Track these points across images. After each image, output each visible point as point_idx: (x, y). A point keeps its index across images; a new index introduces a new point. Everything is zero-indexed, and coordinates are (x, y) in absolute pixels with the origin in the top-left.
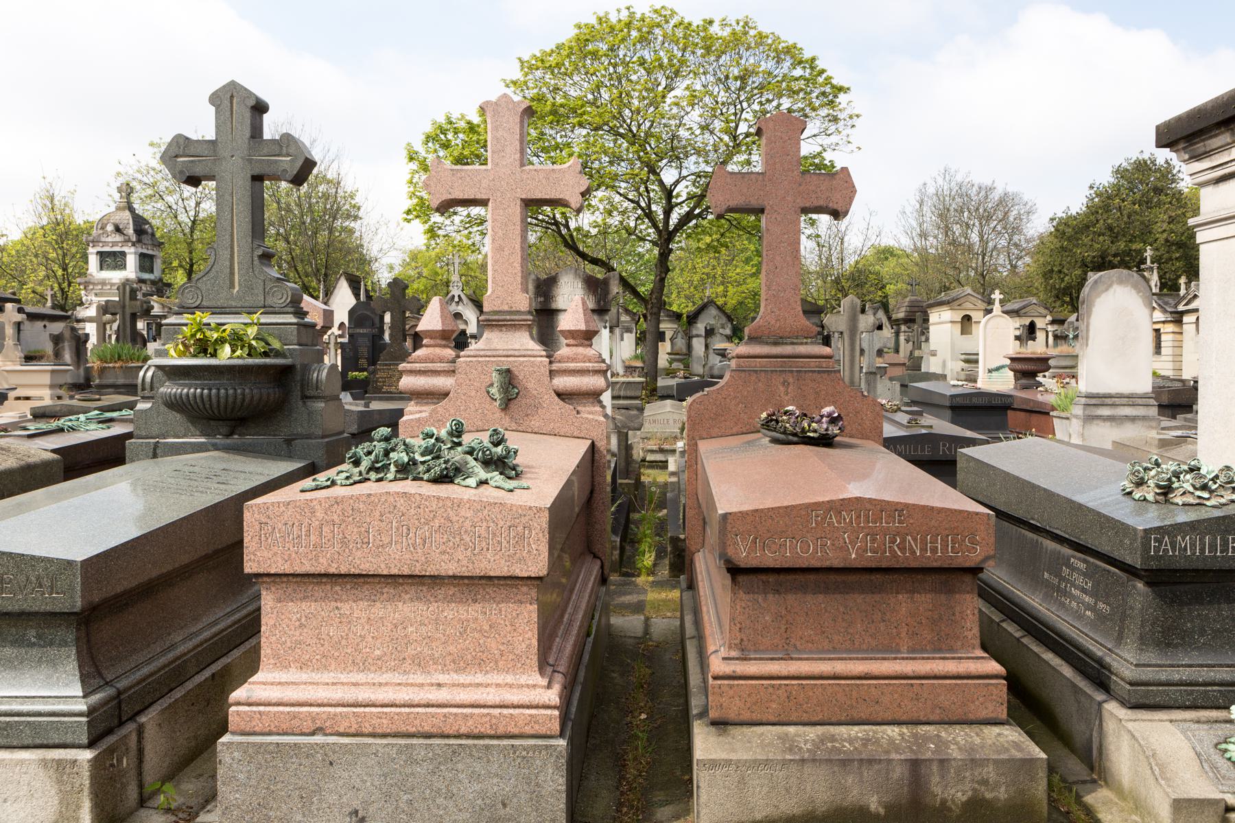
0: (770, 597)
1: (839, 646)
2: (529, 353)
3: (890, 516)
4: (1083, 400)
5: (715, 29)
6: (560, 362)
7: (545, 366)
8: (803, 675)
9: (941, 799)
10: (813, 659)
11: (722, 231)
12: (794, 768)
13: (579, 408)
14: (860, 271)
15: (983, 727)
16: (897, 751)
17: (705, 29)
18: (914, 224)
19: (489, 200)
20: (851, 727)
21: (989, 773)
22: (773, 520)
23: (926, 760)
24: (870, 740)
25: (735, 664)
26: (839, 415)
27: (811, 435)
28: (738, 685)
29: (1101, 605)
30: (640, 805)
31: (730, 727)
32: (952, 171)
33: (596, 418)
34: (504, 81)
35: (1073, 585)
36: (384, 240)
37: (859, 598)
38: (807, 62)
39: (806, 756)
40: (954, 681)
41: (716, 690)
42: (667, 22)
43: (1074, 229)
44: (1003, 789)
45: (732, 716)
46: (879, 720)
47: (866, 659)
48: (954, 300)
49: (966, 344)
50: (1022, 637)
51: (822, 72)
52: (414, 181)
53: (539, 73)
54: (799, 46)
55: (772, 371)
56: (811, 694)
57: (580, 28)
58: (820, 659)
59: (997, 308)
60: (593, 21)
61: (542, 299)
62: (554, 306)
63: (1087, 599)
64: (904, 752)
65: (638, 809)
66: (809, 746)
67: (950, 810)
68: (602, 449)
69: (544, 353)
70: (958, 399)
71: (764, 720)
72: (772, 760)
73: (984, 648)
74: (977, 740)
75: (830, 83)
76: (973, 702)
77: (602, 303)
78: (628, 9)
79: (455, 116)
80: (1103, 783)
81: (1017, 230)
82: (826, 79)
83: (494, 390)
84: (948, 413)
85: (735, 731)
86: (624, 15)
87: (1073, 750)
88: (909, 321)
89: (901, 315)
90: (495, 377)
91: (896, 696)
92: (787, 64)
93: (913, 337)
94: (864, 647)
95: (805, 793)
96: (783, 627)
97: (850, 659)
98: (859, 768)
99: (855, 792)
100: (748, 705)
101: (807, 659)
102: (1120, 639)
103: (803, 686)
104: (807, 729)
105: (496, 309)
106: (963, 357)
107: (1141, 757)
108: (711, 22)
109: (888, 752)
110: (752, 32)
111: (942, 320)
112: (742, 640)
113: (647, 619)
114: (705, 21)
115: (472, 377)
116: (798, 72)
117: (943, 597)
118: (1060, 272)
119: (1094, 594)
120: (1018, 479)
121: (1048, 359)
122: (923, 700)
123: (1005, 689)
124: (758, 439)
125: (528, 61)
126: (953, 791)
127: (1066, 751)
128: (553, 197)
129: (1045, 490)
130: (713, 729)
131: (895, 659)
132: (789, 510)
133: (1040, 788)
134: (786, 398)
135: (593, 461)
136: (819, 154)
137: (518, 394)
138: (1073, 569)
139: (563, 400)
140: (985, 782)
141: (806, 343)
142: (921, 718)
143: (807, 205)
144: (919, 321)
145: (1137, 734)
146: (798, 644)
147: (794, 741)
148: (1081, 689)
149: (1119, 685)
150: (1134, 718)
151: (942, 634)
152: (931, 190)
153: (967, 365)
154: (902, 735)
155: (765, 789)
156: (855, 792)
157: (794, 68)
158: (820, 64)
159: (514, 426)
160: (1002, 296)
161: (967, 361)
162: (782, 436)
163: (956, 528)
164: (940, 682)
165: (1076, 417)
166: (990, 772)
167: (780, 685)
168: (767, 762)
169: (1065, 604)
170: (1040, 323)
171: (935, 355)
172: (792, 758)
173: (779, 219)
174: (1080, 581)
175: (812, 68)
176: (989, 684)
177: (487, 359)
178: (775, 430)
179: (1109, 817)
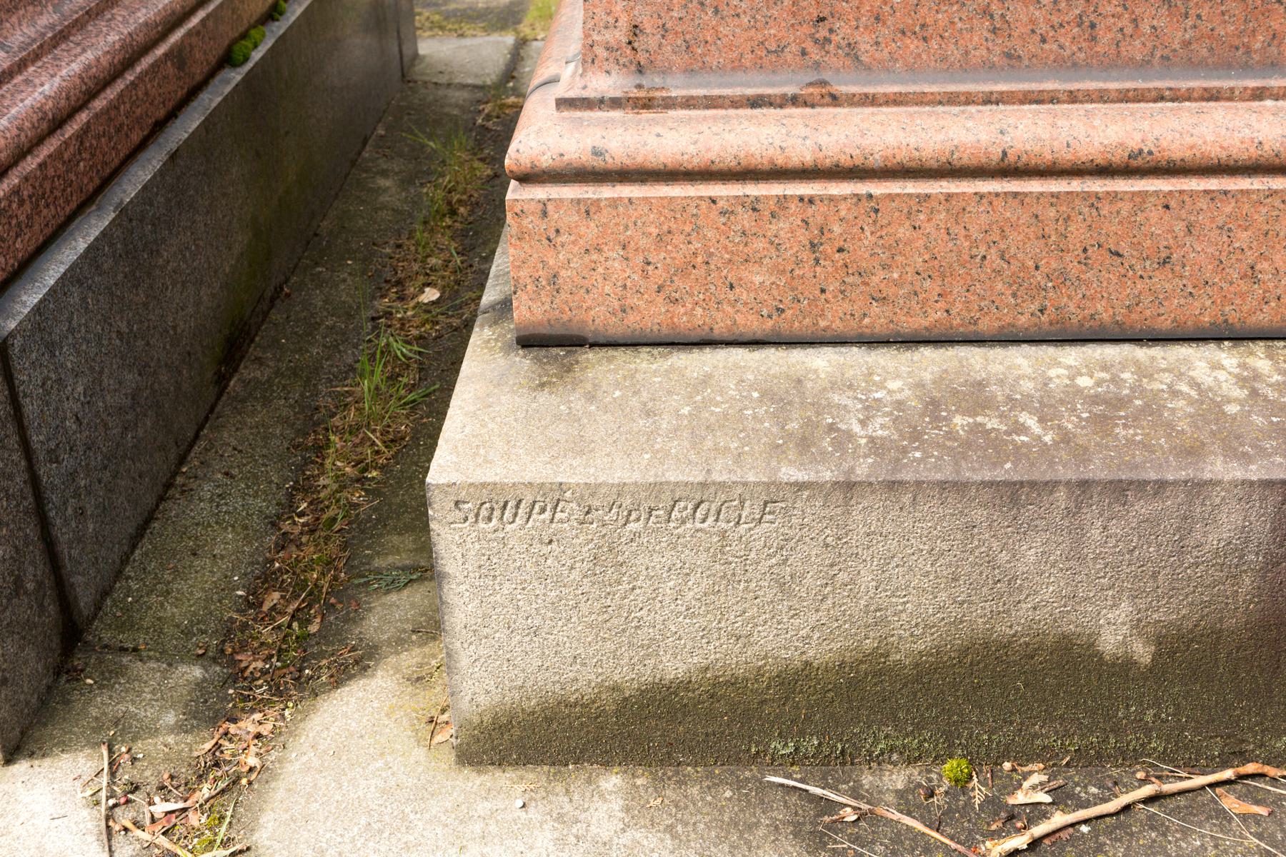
1: (1033, 46)
8: (876, 161)
10: (921, 100)
12: (809, 510)
16: (1233, 450)
20: (1050, 350)
24: (1121, 402)
25: (606, 124)
28: (614, 203)
30: (325, 583)
31: (590, 355)
39: (863, 469)
46: (1165, 324)
56: (904, 232)
58: (951, 99)
64: (1262, 452)
65: (313, 598)
66: (880, 427)
72: (722, 485)
85: (597, 366)
91: (1242, 238)
94: (1136, 49)
95: (853, 596)
97: (1073, 98)
99: (1047, 593)
100: (658, 276)
101: (897, 101)
103: (874, 206)
104: (882, 358)
109: (1193, 452)
112: (635, 29)
113: (522, 43)
130: (523, 362)
131: (1259, 95)
146: (864, 43)
154: (1249, 380)
167: (783, 200)
172: (802, 476)
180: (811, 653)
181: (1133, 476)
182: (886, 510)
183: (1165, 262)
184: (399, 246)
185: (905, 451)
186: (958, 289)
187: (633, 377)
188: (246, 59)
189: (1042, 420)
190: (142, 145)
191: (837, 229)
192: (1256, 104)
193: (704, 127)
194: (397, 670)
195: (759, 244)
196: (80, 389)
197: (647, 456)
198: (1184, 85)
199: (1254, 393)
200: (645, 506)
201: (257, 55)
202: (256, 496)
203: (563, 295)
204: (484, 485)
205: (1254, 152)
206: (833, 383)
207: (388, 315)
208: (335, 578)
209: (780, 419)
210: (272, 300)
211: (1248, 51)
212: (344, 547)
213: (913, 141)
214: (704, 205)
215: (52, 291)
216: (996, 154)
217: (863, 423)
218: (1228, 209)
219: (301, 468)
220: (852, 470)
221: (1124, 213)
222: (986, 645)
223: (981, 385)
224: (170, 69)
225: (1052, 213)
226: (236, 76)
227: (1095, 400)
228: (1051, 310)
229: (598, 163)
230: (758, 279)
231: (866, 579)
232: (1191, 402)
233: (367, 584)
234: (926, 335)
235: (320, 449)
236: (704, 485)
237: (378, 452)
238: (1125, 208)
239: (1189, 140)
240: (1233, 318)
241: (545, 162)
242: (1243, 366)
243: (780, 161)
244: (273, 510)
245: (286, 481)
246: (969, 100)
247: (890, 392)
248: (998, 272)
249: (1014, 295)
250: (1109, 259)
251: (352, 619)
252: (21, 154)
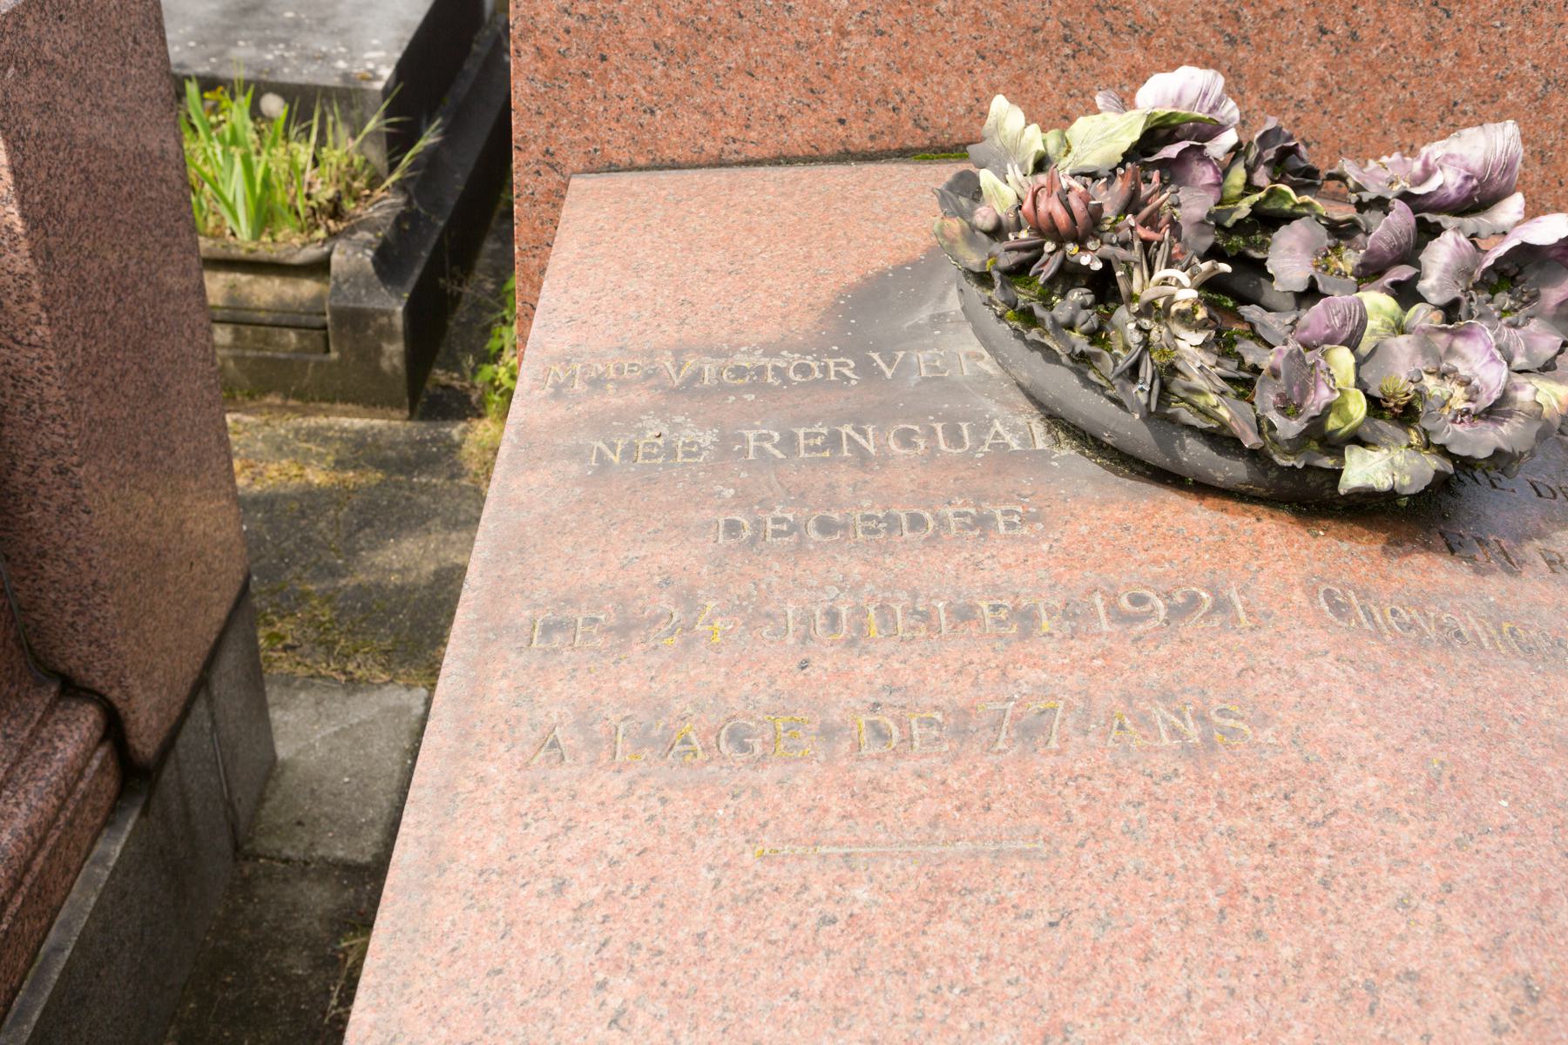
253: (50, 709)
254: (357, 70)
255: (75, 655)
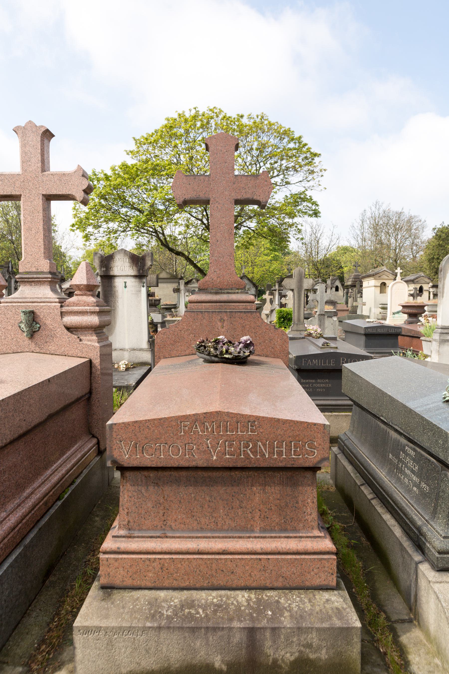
0: (151, 488)
2: (47, 300)
3: (244, 426)
4: (440, 330)
5: (245, 121)
6: (68, 306)
7: (57, 309)
8: (173, 551)
9: (273, 659)
10: (183, 537)
11: (250, 236)
12: (152, 633)
13: (82, 338)
14: (328, 259)
15: (316, 592)
17: (238, 120)
18: (359, 233)
19: (21, 195)
21: (312, 638)
22: (150, 429)
23: (260, 628)
26: (251, 342)
27: (227, 356)
28: (121, 559)
29: (423, 485)
30: (56, 643)
31: (115, 591)
32: (380, 203)
33: (93, 344)
34: (126, 151)
35: (406, 466)
36: (68, 243)
37: (222, 490)
38: (296, 139)
40: (294, 557)
41: (105, 562)
42: (217, 116)
43: (446, 234)
44: (324, 651)
45: (117, 582)
46: (234, 586)
47: (226, 537)
48: (376, 274)
49: (382, 298)
50: (372, 499)
51: (306, 145)
52: (76, 208)
53: (145, 147)
54: (292, 130)
55: (213, 312)
57: (168, 120)
58: (190, 537)
59: (399, 277)
60: (176, 116)
61: (104, 269)
62: (112, 273)
63: (415, 478)
67: (280, 667)
68: (97, 365)
69: (57, 300)
70: (369, 330)
71: (143, 585)
72: (134, 627)
73: (321, 528)
74: (308, 607)
75: (310, 151)
76: (309, 573)
77: (141, 271)
78: (195, 108)
79: (98, 171)
80: (417, 623)
81: (416, 237)
82: (307, 149)
83: (23, 326)
84: (363, 338)
86: (193, 112)
87: (399, 591)
88: (353, 286)
89: (349, 283)
90: (22, 317)
91: (247, 568)
92: (286, 140)
93: (353, 295)
94: (226, 527)
95: (162, 653)
96: (161, 512)
97: (213, 537)
98: (205, 634)
99: (202, 653)
100: (130, 574)
102: (434, 514)
105: (27, 270)
106: (381, 306)
107: (443, 616)
108: (242, 116)
110: (266, 122)
111: (370, 285)
112: (129, 522)
114: (238, 115)
115: (8, 316)
116: (292, 145)
117: (289, 489)
118: (438, 259)
119: (419, 475)
120: (374, 387)
121: (424, 306)
122: (269, 571)
123: (335, 563)
124: (195, 359)
125: (139, 140)
126: (283, 653)
127: (395, 590)
128: (64, 193)
129: (390, 396)
131: (249, 537)
132: (162, 421)
133: (355, 650)
134: (223, 330)
135: (91, 373)
136: (304, 192)
137: (39, 328)
138: (407, 455)
139: (71, 332)
140: (309, 646)
141: (238, 293)
142: (268, 585)
143: (239, 197)
144: (358, 286)
145: (441, 597)
146: (173, 525)
147: (160, 606)
148: (405, 548)
149: (431, 551)
150: (440, 580)
151: (288, 517)
152: (368, 214)
153: (383, 310)
155: (129, 650)
156: (202, 653)
157: (289, 143)
158: (304, 140)
159: (38, 350)
160: (401, 271)
161: (383, 308)
162: (208, 357)
163: (297, 436)
164: (283, 557)
165: (435, 340)
166: (313, 638)
168: (130, 629)
169: (401, 479)
170: (425, 287)
171: (365, 305)
173: (219, 208)
174: (411, 464)
175: (300, 143)
176: (322, 559)
177: (19, 304)
178: (203, 353)
179: (417, 659)
180: (153, 667)
181: (217, 626)
182: (168, 634)
183: (233, 572)
184: (96, 539)
185: (173, 619)
186: (191, 578)
187: (123, 597)
188: (63, 498)
189: (203, 611)
190: (33, 527)
191: (166, 565)
192: (249, 539)
193: (140, 543)
194: (67, 669)
195: (151, 568)
196: (7, 593)
197: (120, 619)
198: (235, 535)
199: (249, 604)
200: (118, 632)
201: (66, 496)
202: (46, 616)
203: (111, 578)
204: (85, 626)
205: (247, 551)
206: (163, 600)
207: (89, 561)
208: (59, 641)
209: (150, 609)
210: (62, 556)
211: (247, 528)
212: (63, 632)
213: (180, 547)
214: (139, 559)
215: (5, 571)
216: (197, 550)
217: (167, 611)
218: (243, 562)
219: (58, 608)
220: (161, 624)
221: (223, 562)
222: (191, 666)
223: (193, 601)
224: (43, 507)
225: (209, 562)
226: (59, 503)
227: (216, 605)
228: (211, 583)
229: (118, 550)
230: (150, 575)
231: (164, 649)
232: (235, 606)
233: (66, 643)
234: (185, 588)
235: (64, 602)
236: (130, 627)
237: (77, 604)
238: (223, 561)
239: (234, 548)
240: (248, 584)
241: (108, 550)
242: (249, 596)
243: (154, 551)
244: (49, 621)
245: (54, 611)
246: (193, 537)
247: (175, 603)
248: (199, 574)
249: (203, 579)
250: (221, 572)
251: (60, 654)
252: (4, 538)
253: (90, 438)
254: (129, 384)
255: (95, 431)
